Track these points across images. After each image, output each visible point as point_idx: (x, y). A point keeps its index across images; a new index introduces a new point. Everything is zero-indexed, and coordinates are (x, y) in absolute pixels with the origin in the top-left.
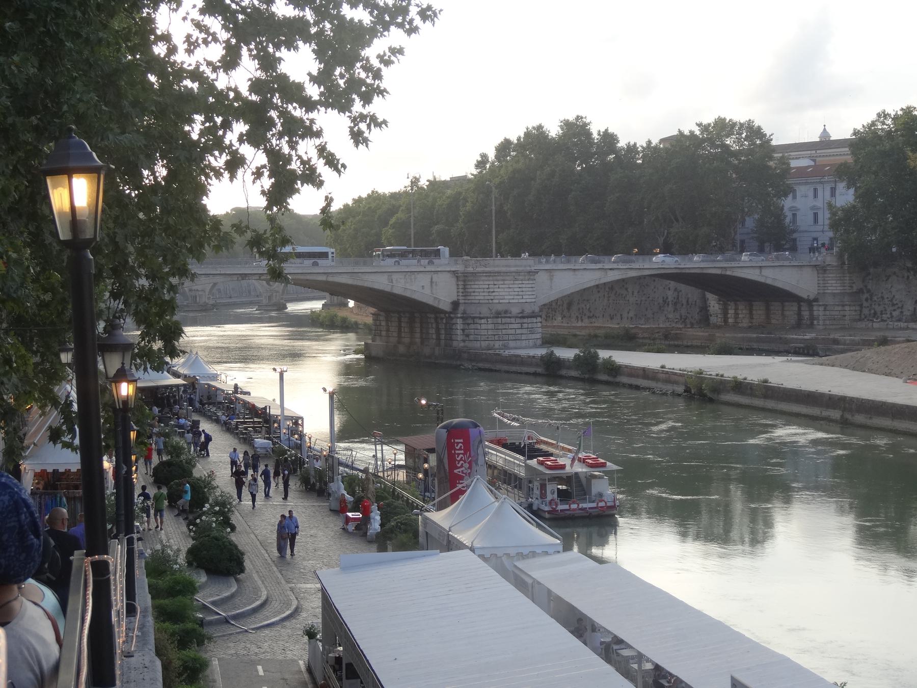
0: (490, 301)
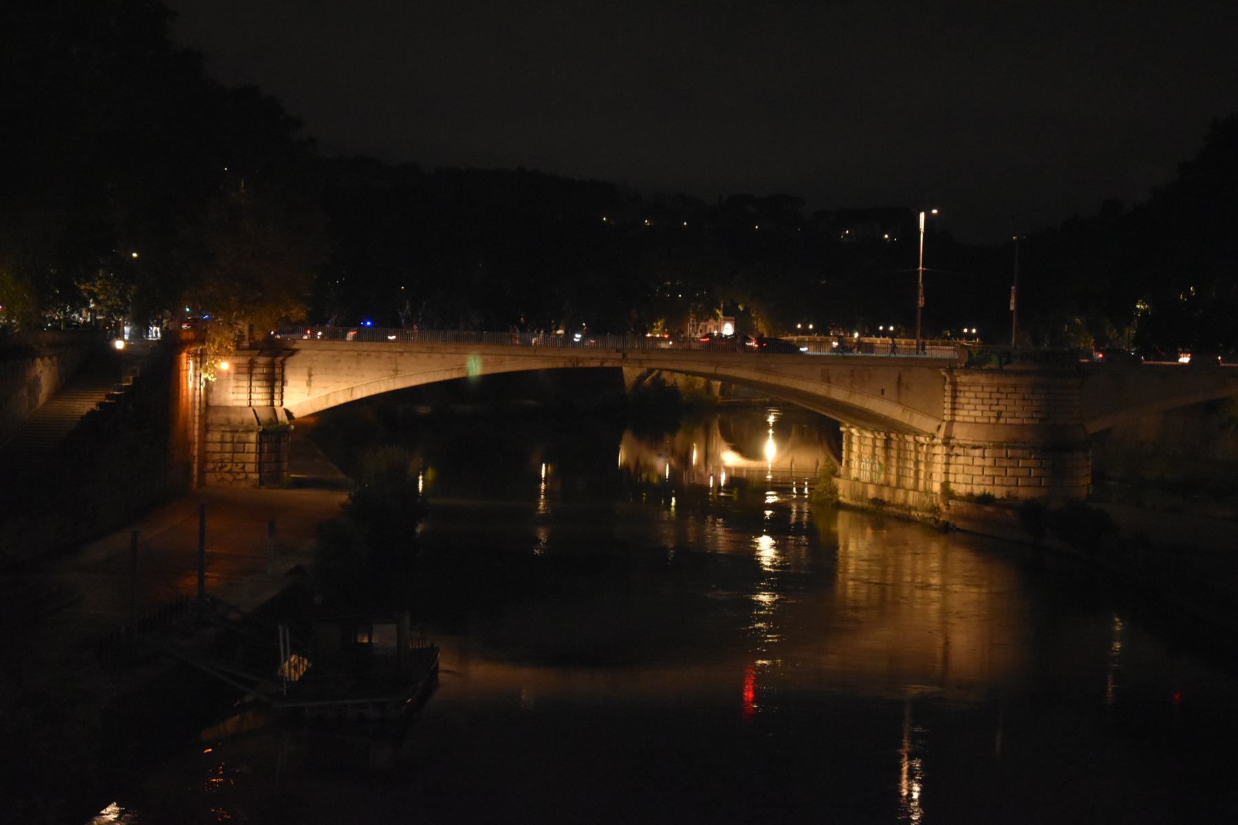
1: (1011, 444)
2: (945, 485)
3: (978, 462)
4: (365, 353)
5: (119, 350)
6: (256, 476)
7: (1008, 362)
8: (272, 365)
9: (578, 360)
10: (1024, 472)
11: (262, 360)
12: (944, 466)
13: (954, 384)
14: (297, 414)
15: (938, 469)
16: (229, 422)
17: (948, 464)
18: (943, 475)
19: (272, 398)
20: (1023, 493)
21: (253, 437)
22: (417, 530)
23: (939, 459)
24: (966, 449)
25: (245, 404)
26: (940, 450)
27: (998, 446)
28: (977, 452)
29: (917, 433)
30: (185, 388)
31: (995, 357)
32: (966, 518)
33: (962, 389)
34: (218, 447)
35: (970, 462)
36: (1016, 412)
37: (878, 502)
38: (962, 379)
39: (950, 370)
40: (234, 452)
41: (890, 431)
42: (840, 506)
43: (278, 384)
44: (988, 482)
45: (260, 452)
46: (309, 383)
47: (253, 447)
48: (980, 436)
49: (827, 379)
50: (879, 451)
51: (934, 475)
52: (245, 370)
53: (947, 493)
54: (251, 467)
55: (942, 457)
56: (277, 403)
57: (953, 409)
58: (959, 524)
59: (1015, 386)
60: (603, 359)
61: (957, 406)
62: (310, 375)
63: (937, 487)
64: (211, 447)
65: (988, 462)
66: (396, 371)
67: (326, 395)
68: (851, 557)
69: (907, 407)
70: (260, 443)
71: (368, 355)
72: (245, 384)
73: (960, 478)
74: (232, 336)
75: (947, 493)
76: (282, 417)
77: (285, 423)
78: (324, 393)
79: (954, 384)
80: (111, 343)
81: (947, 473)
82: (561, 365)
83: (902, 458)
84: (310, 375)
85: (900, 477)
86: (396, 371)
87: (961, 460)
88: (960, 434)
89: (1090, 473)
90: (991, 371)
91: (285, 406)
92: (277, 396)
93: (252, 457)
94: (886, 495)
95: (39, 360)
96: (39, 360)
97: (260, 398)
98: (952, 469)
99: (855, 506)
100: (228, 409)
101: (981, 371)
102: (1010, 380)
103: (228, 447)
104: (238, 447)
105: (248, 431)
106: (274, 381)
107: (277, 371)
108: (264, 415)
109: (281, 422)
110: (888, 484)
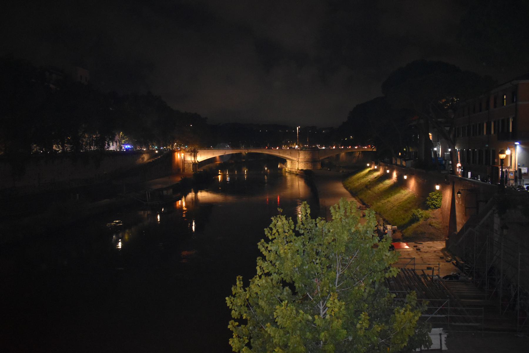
1: (307, 161)
2: (298, 168)
3: (302, 164)
5: (404, 178)
6: (192, 170)
7: (306, 149)
8: (195, 154)
9: (241, 151)
10: (309, 166)
11: (193, 153)
13: (299, 153)
14: (199, 161)
15: (297, 166)
16: (188, 163)
19: (195, 159)
20: (309, 169)
21: (192, 165)
23: (297, 164)
25: (190, 160)
26: (297, 163)
27: (305, 162)
28: (302, 163)
29: (295, 160)
30: (177, 157)
31: (304, 149)
32: (300, 173)
34: (186, 166)
36: (308, 157)
37: (290, 171)
38: (300, 152)
39: (298, 151)
40: (189, 167)
41: (292, 160)
42: (286, 172)
43: (196, 157)
45: (193, 167)
46: (201, 156)
47: (192, 166)
48: (302, 160)
49: (279, 153)
50: (291, 164)
52: (190, 155)
53: (298, 169)
54: (191, 169)
56: (196, 160)
57: (299, 156)
58: (299, 174)
59: (307, 153)
62: (201, 155)
63: (297, 168)
64: (185, 167)
65: (304, 164)
66: (214, 154)
68: (184, 158)
69: (292, 157)
70: (193, 165)
72: (190, 157)
73: (300, 167)
75: (298, 169)
76: (197, 162)
78: (204, 157)
79: (299, 153)
81: (298, 166)
82: (238, 152)
83: (293, 164)
84: (201, 155)
85: (293, 167)
86: (214, 154)
87: (300, 164)
88: (300, 160)
89: (508, 181)
90: (304, 151)
91: (197, 160)
92: (196, 159)
93: (192, 168)
94: (291, 170)
95: (395, 276)
96: (395, 276)
97: (193, 159)
98: (299, 165)
100: (188, 161)
101: (302, 151)
102: (306, 152)
103: (188, 166)
104: (189, 166)
105: (191, 164)
106: (195, 156)
107: (196, 155)
108: (193, 162)
110: (292, 168)
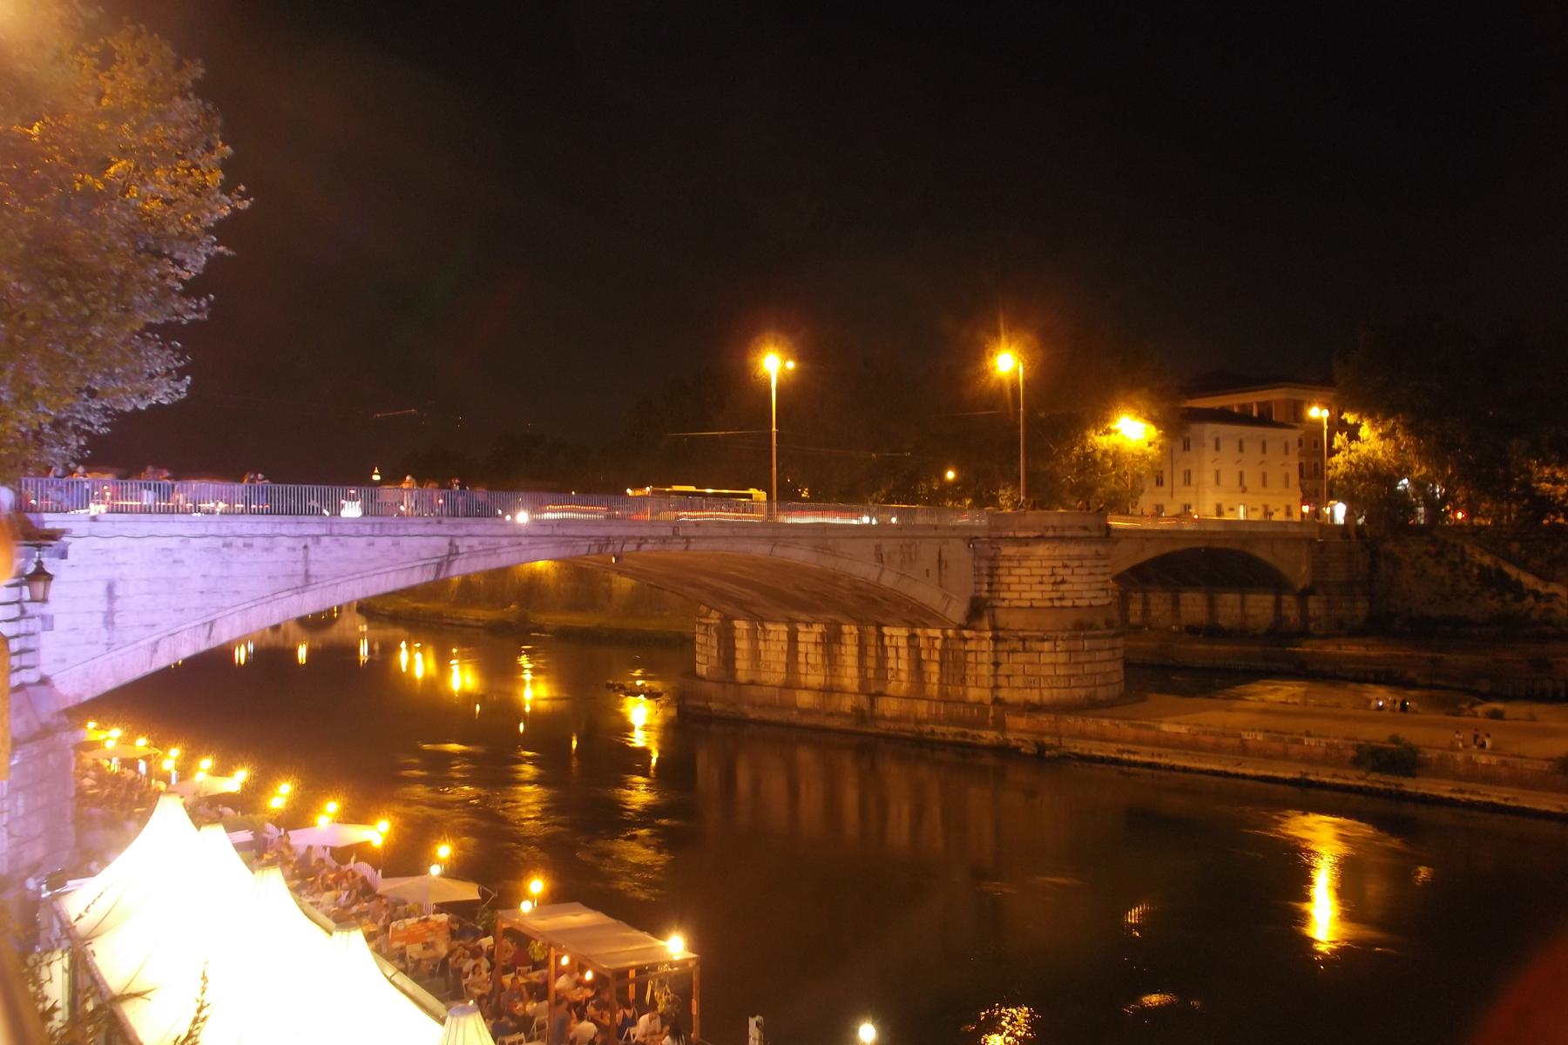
0: (1057, 603)
4: (240, 542)
12: (992, 667)
17: (997, 664)
18: (992, 679)
22: (91, 725)
24: (1027, 643)
33: (1007, 564)
35: (1036, 660)
44: (1063, 685)
51: (968, 678)
55: (989, 655)
60: (641, 538)
61: (995, 587)
67: (152, 644)
71: (245, 545)
74: (94, 49)
77: (570, 1031)
80: (481, 692)
98: (1003, 670)
99: (1221, 772)
109: (466, 1011)
